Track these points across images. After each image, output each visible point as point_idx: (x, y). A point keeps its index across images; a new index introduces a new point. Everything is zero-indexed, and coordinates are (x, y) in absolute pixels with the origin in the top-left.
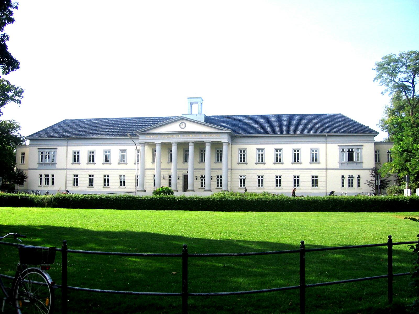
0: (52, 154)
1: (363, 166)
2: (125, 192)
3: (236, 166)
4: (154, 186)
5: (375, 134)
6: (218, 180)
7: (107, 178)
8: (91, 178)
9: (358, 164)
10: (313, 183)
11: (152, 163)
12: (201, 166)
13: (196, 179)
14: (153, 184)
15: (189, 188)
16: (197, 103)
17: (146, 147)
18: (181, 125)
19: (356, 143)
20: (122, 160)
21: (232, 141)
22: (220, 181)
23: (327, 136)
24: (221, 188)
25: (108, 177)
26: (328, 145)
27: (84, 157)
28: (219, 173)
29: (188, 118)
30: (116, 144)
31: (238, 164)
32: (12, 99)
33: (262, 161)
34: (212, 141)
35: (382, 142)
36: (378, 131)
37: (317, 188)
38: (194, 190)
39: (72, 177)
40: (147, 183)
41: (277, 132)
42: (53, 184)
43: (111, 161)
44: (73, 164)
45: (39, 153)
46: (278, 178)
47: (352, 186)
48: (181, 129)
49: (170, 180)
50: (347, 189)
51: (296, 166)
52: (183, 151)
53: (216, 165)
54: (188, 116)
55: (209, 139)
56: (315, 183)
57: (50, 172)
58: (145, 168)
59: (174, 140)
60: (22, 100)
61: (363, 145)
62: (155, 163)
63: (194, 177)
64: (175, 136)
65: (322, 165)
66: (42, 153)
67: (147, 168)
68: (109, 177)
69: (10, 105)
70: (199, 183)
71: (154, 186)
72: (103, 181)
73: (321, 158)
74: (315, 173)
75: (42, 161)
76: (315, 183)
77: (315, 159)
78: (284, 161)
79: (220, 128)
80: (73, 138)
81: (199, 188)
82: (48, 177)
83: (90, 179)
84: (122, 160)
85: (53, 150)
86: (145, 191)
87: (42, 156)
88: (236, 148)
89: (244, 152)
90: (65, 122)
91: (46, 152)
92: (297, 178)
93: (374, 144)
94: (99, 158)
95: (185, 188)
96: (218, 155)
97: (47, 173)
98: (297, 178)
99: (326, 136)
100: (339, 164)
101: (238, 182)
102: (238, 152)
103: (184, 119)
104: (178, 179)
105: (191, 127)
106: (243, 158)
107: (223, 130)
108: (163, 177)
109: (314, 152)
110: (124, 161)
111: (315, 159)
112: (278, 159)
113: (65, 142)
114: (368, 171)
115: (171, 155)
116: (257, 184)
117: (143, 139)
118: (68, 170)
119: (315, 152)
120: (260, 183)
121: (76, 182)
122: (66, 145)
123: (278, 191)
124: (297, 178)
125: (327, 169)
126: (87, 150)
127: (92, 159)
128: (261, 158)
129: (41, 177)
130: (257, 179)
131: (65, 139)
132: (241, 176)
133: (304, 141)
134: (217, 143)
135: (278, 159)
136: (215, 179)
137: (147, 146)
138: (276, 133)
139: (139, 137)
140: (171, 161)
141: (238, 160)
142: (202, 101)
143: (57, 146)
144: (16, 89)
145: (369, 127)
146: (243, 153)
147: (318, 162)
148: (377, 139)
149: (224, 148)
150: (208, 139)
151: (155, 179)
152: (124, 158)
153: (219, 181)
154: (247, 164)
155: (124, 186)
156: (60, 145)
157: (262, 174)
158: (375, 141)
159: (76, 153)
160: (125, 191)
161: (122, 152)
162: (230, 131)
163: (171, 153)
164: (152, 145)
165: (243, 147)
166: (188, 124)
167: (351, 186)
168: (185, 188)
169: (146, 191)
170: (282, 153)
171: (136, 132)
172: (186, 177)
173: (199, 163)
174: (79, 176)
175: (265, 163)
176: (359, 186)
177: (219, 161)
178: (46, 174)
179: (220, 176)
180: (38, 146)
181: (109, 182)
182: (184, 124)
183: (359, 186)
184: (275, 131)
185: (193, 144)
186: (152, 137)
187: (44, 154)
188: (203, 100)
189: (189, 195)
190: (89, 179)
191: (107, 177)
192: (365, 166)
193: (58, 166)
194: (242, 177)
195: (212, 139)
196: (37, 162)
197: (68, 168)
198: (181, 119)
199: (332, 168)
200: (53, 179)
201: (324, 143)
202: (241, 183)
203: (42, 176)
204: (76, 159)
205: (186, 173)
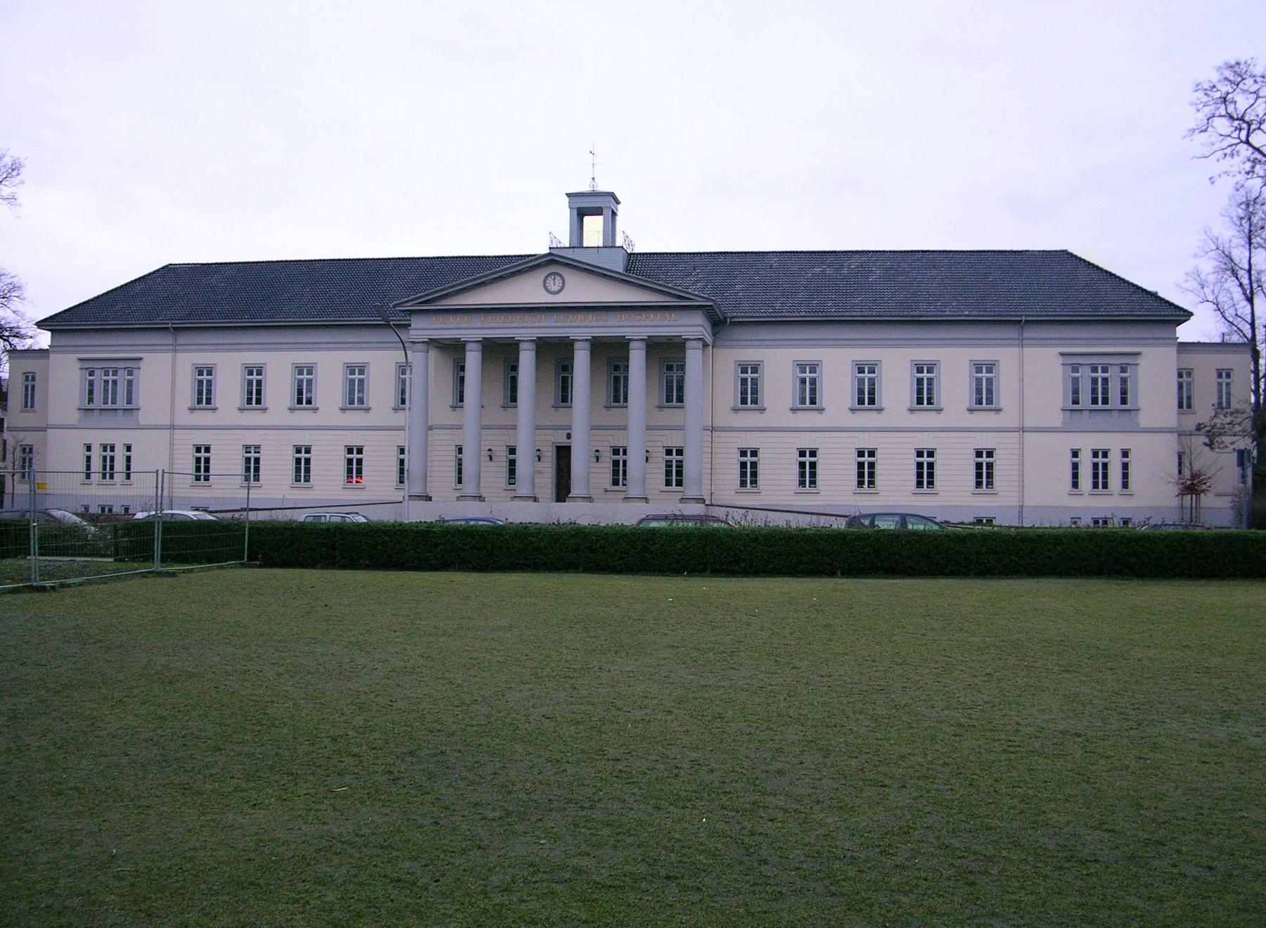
1: (140, 419)
2: (365, 500)
3: (725, 417)
4: (460, 481)
5: (1183, 315)
6: (669, 465)
8: (203, 455)
11: (451, 407)
12: (614, 416)
13: (491, 459)
14: (454, 474)
15: (577, 489)
16: (597, 211)
17: (433, 353)
19: (1121, 345)
20: (355, 396)
21: (714, 335)
22: (677, 466)
23: (1026, 321)
24: (679, 488)
25: (308, 451)
26: (1028, 351)
27: (229, 388)
28: (674, 441)
29: (572, 260)
30: (335, 346)
31: (735, 410)
33: (813, 402)
34: (432, 337)
35: (1199, 344)
36: (1190, 309)
37: (814, 490)
38: (480, 497)
40: (434, 474)
43: (319, 401)
44: (192, 409)
47: (1105, 486)
48: (545, 292)
49: (512, 463)
50: (1086, 494)
51: (925, 419)
53: (293, 414)
54: (569, 254)
55: (642, 330)
56: (984, 475)
57: (118, 438)
58: (429, 424)
59: (525, 330)
61: (1138, 354)
63: (483, 453)
64: (528, 319)
65: (1008, 418)
66: (91, 374)
68: (312, 452)
71: (460, 481)
72: (291, 465)
74: (985, 442)
75: (91, 400)
76: (984, 475)
77: (984, 396)
78: (883, 403)
80: (1041, 318)
81: (606, 491)
84: (355, 396)
85: (130, 364)
86: (430, 499)
87: (91, 384)
88: (730, 358)
89: (755, 370)
90: (169, 271)
91: (107, 374)
92: (866, 459)
93: (1174, 350)
94: (279, 389)
95: (562, 491)
96: (669, 383)
98: (984, 460)
99: (1021, 321)
100: (1061, 412)
101: (607, 470)
102: (736, 372)
103: (554, 260)
104: (595, 460)
105: (580, 290)
106: (749, 394)
108: (490, 453)
109: (982, 372)
110: (361, 401)
111: (984, 396)
112: (867, 397)
113: (168, 339)
114: (1169, 436)
115: (462, 379)
117: (423, 328)
118: (176, 431)
119: (984, 375)
121: (749, 473)
122: (171, 347)
123: (866, 503)
124: (928, 457)
125: (1023, 430)
126: (909, 363)
127: (254, 395)
128: (809, 395)
129: (128, 453)
131: (168, 328)
133: (930, 339)
134: (665, 341)
135: (867, 397)
136: (607, 458)
137: (436, 350)
140: (514, 398)
142: (615, 204)
143: (141, 351)
146: (749, 375)
147: (994, 406)
148: (1185, 333)
149: (693, 357)
150: (637, 329)
151: (460, 460)
152: (361, 390)
154: (763, 410)
155: (309, 481)
156: (152, 348)
157: (871, 446)
158: (1179, 340)
159: (252, 375)
160: (362, 498)
161: (355, 370)
162: (712, 303)
163: (513, 374)
164: (453, 350)
165: (750, 355)
166: (571, 277)
167: (1100, 486)
168: (562, 491)
170: (938, 377)
172: (563, 454)
173: (608, 408)
175: (823, 410)
176: (1125, 485)
177: (923, 404)
180: (81, 352)
181: (312, 468)
182: (558, 278)
183: (1125, 485)
185: (645, 346)
186: (452, 321)
187: (99, 377)
188: (618, 202)
189: (576, 513)
191: (358, 453)
193: (144, 417)
195: (652, 329)
196: (77, 405)
197: (178, 423)
200: (1125, 466)
201: (1013, 345)
203: (116, 449)
204: (204, 396)
205: (562, 440)
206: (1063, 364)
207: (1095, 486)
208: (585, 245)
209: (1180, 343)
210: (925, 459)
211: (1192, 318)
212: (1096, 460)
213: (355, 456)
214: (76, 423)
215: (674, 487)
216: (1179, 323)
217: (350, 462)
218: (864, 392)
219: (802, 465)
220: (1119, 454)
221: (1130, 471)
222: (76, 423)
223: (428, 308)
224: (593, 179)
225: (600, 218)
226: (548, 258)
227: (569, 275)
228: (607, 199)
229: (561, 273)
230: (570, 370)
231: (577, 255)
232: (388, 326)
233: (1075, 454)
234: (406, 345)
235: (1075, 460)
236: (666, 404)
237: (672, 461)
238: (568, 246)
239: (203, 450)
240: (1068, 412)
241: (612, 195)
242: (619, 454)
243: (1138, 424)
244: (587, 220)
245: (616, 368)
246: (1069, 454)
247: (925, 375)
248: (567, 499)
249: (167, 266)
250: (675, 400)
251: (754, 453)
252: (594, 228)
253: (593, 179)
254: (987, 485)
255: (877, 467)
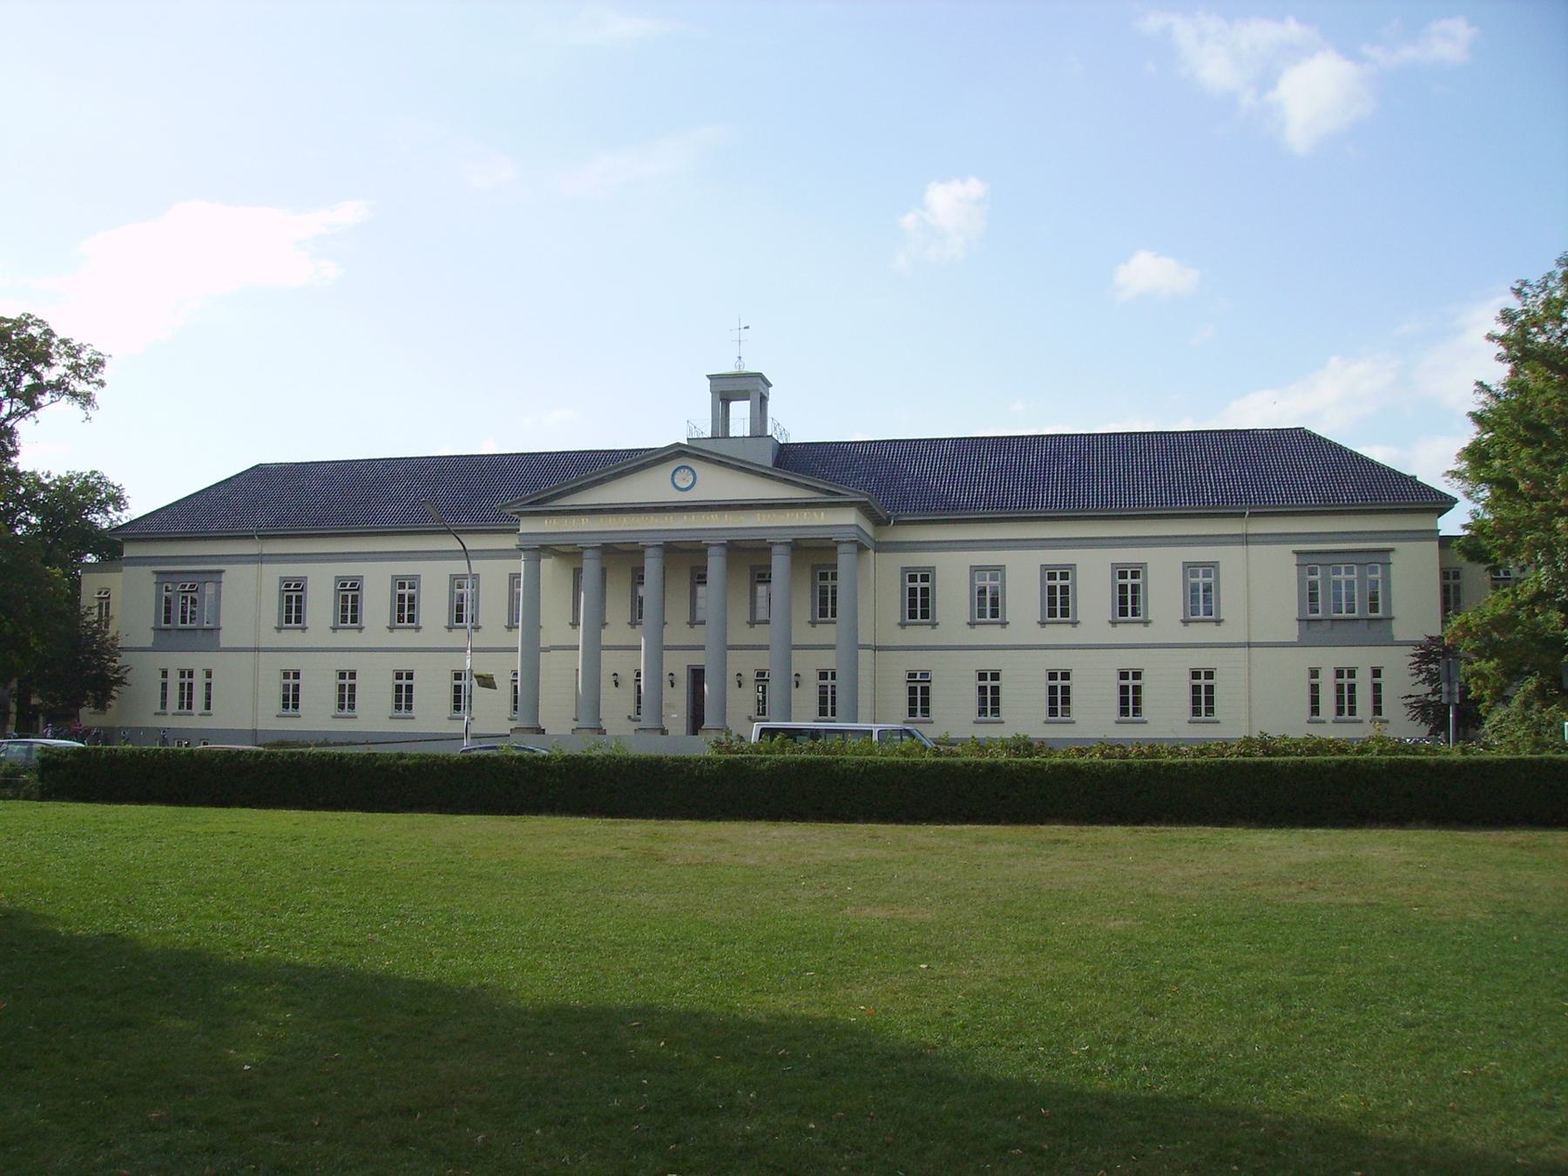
0: (977, 583)
5: (1443, 504)
7: (347, 681)
9: (1313, 624)
10: (1196, 701)
17: (547, 565)
18: (678, 476)
32: (59, 387)
39: (1044, 678)
41: (1051, 503)
42: (208, 706)
45: (1298, 570)
46: (1059, 683)
47: (1352, 711)
51: (1129, 632)
52: (629, 575)
53: (974, 628)
54: (710, 447)
56: (1202, 699)
60: (99, 395)
61: (220, 572)
62: (518, 628)
67: (261, 646)
69: (54, 410)
70: (525, 698)
72: (974, 696)
73: (1230, 600)
76: (1202, 699)
79: (827, 488)
82: (190, 679)
83: (344, 685)
89: (925, 578)
90: (261, 475)
97: (186, 666)
102: (903, 580)
104: (794, 684)
105: (715, 484)
106: (919, 604)
107: (840, 494)
116: (1188, 705)
120: (989, 699)
121: (291, 699)
127: (405, 610)
128: (989, 605)
129: (164, 680)
130: (973, 684)
132: (912, 675)
138: (966, 509)
139: (517, 527)
141: (903, 611)
144: (74, 352)
145: (1418, 479)
148: (1452, 524)
149: (844, 560)
153: (827, 693)
154: (1004, 624)
157: (1136, 666)
158: (1441, 534)
162: (866, 499)
169: (544, 730)
170: (1145, 582)
171: (509, 504)
174: (415, 674)
176: (1377, 710)
177: (916, 618)
178: (183, 667)
179: (347, 674)
181: (414, 697)
183: (1377, 710)
184: (1043, 500)
185: (790, 549)
188: (769, 385)
190: (340, 685)
192: (1400, 631)
193: (225, 639)
194: (918, 678)
198: (676, 452)
199: (957, 644)
200: (1377, 688)
202: (912, 702)
204: (293, 607)
206: (1297, 565)
207: (1340, 711)
208: (731, 435)
209: (1441, 536)
210: (1130, 682)
211: (1456, 505)
212: (1340, 681)
213: (404, 682)
214: (151, 645)
215: (989, 717)
216: (1441, 512)
217: (342, 687)
218: (1127, 600)
219: (982, 690)
220: (1369, 673)
221: (414, 694)
222: (151, 645)
223: (538, 509)
224: (740, 358)
225: (748, 403)
226: (676, 450)
227: (701, 469)
228: (755, 380)
229: (690, 465)
230: (1457, 570)
231: (722, 448)
232: (448, 532)
233: (1314, 673)
234: (469, 554)
235: (1314, 681)
236: (285, 625)
237: (827, 686)
238: (710, 436)
239: (1203, 675)
240: (1305, 623)
241: (760, 376)
242: (1056, 679)
243: (1392, 636)
244: (735, 407)
245: (824, 577)
246: (1307, 674)
247: (1058, 583)
248: (699, 731)
249: (257, 466)
250: (919, 616)
251: (1066, 676)
252: (740, 416)
253: (740, 358)
254: (1134, 712)
255: (1144, 691)
